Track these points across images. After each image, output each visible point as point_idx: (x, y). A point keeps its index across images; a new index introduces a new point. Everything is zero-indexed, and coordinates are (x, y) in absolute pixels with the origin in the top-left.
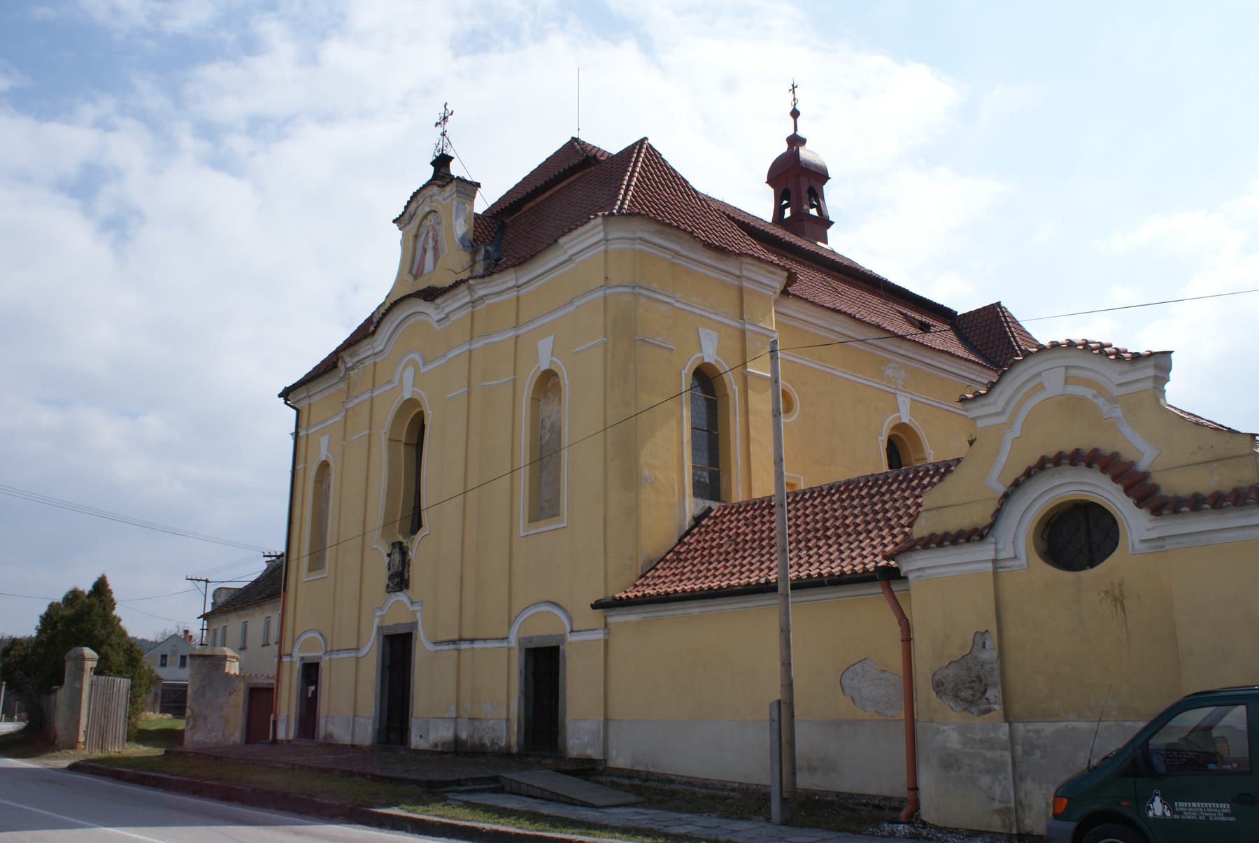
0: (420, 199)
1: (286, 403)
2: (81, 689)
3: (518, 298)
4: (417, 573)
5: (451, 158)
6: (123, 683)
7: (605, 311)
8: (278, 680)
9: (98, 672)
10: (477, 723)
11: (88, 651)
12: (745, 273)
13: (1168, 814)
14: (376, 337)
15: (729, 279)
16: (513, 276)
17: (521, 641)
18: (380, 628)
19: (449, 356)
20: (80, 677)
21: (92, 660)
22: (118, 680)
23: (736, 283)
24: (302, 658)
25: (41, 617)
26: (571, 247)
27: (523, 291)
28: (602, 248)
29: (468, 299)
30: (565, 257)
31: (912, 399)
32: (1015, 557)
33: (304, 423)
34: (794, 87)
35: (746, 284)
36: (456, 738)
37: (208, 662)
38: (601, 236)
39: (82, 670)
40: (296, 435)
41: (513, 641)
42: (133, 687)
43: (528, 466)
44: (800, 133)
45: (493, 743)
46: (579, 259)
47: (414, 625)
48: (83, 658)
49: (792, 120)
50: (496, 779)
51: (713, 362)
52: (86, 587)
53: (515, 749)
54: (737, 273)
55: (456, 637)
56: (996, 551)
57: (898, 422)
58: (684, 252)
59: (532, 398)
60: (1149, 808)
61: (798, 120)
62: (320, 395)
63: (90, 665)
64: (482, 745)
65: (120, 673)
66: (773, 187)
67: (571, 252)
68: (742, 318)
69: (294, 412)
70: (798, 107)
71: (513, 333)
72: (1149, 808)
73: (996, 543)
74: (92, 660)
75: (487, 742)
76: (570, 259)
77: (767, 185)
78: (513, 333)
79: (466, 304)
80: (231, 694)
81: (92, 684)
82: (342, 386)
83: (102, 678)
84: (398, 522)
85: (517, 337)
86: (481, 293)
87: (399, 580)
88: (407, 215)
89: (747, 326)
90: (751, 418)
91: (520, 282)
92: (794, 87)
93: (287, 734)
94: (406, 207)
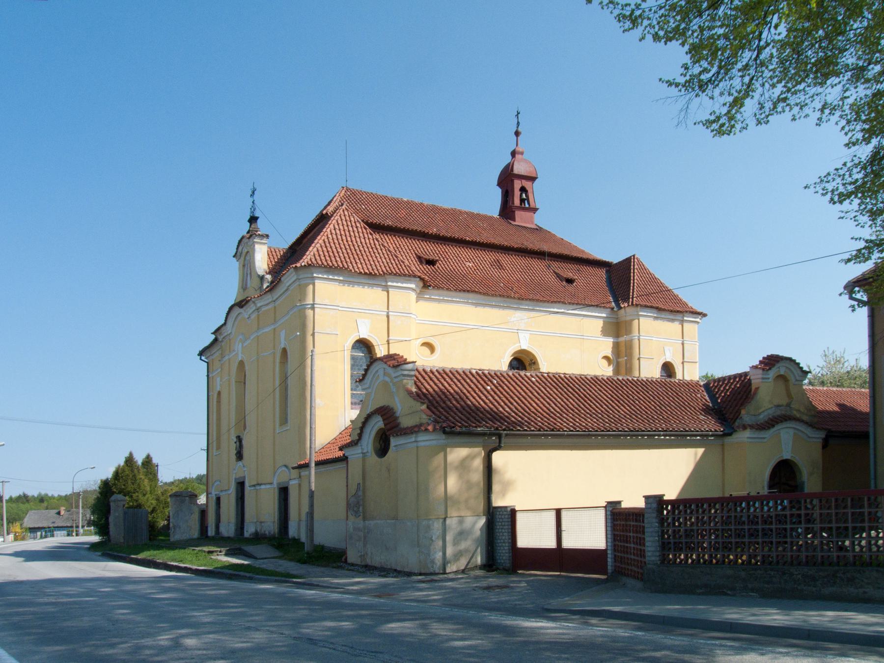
0: (242, 243)
1: (201, 359)
3: (275, 307)
4: (246, 452)
8: (207, 506)
10: (263, 524)
12: (389, 284)
14: (227, 324)
16: (270, 296)
17: (279, 484)
18: (235, 479)
19: (252, 338)
24: (216, 495)
25: (101, 481)
26: (288, 281)
27: (278, 303)
28: (298, 283)
29: (254, 308)
30: (284, 289)
31: (530, 334)
32: (368, 452)
33: (211, 370)
34: (518, 113)
36: (256, 531)
37: (179, 498)
40: (208, 376)
41: (275, 485)
44: (520, 149)
45: (269, 533)
46: (291, 288)
47: (244, 477)
49: (516, 138)
50: (240, 549)
52: (122, 462)
53: (277, 536)
55: (255, 483)
56: (362, 449)
57: (520, 349)
59: (280, 362)
61: (519, 138)
62: (216, 353)
64: (265, 534)
66: (501, 188)
67: (288, 284)
69: (206, 364)
70: (520, 129)
71: (273, 327)
73: (361, 446)
75: (267, 532)
76: (287, 290)
77: (498, 187)
78: (273, 327)
79: (254, 311)
80: (192, 514)
82: (220, 352)
84: (233, 429)
85: (274, 329)
86: (259, 305)
87: (240, 456)
88: (238, 253)
91: (274, 299)
92: (518, 113)
93: (211, 533)
94: (237, 249)
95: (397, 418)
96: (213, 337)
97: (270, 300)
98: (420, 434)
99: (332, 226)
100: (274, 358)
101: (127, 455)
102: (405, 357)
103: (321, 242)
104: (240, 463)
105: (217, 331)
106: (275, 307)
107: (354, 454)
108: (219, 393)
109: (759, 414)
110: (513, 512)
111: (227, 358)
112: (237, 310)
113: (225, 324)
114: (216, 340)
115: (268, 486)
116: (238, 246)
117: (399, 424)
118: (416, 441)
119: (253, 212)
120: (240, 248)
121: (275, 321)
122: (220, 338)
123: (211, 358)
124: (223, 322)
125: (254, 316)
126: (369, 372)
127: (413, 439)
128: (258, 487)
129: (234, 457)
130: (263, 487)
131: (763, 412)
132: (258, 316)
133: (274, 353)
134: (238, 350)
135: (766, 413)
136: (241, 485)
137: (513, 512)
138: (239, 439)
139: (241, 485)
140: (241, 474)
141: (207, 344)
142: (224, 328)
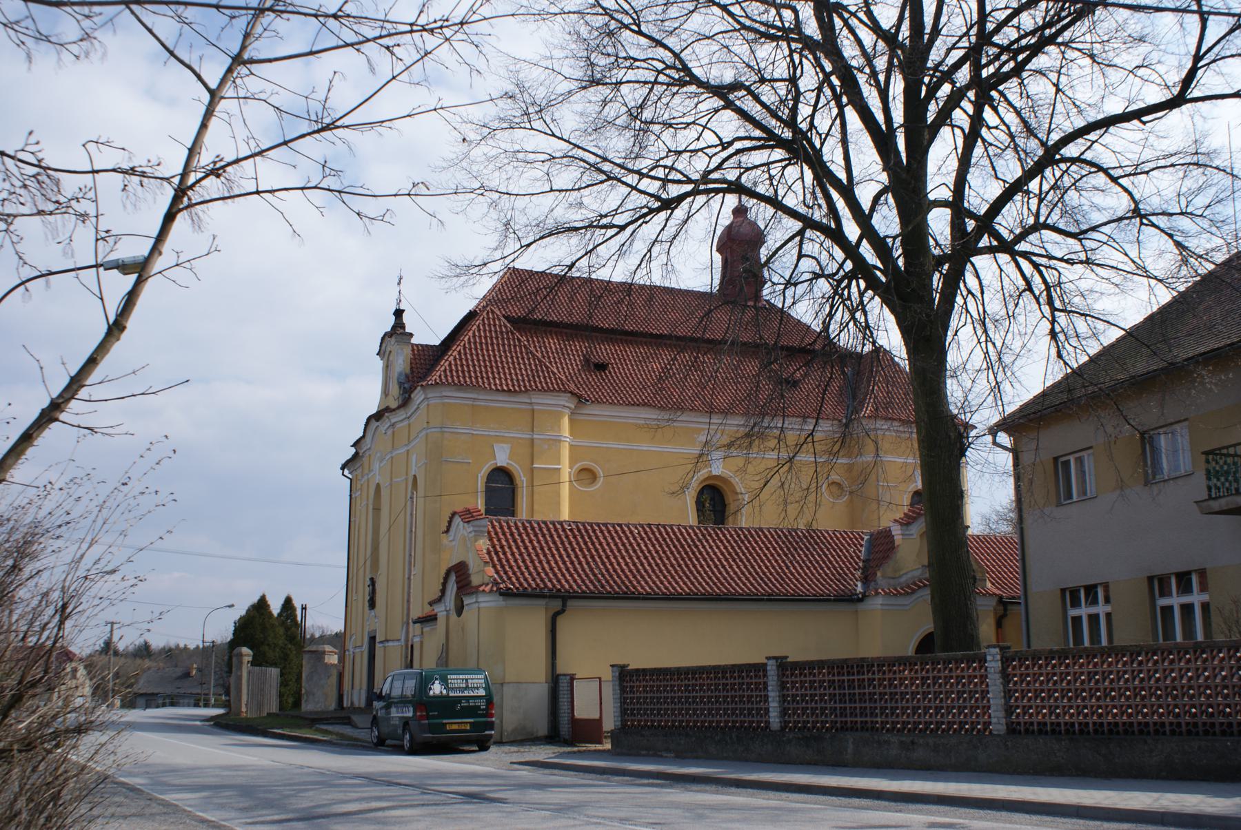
2: (241, 676)
3: (409, 425)
5: (403, 311)
6: (274, 672)
7: (427, 444)
9: (255, 663)
11: (245, 650)
12: (533, 401)
13: (444, 692)
15: (523, 406)
20: (240, 668)
21: (248, 655)
22: (269, 669)
23: (529, 407)
27: (412, 420)
35: (535, 407)
38: (423, 397)
39: (241, 663)
42: (282, 675)
43: (1124, 333)
48: (241, 655)
51: (505, 465)
54: (528, 401)
58: (481, 397)
60: (430, 689)
63: (247, 659)
65: (274, 665)
68: (533, 431)
71: (406, 448)
72: (430, 689)
74: (248, 655)
76: (418, 408)
78: (406, 448)
81: (249, 673)
83: (257, 668)
86: (393, 421)
89: (535, 436)
90: (536, 497)
94: (381, 346)
95: (469, 576)
96: (353, 450)
97: (404, 416)
98: (480, 595)
99: (471, 334)
100: (407, 484)
101: (255, 599)
102: (182, 645)
103: (455, 353)
104: (373, 613)
105: (356, 444)
106: (409, 425)
107: (440, 609)
108: (415, 476)
109: (900, 577)
110: (572, 678)
111: (366, 478)
112: (374, 424)
113: (364, 436)
114: (356, 456)
115: (396, 643)
116: (381, 343)
117: (470, 582)
118: (477, 602)
119: (398, 304)
120: (384, 345)
121: (409, 442)
122: (361, 452)
123: (355, 473)
124: (361, 434)
125: (390, 432)
126: (453, 524)
127: (474, 600)
128: (387, 644)
129: (367, 604)
130: (390, 644)
131: (906, 573)
132: (393, 432)
133: (406, 479)
134: (377, 472)
135: (909, 575)
136: (372, 639)
137: (572, 678)
138: (373, 581)
139: (372, 639)
140: (372, 628)
141: (349, 456)
142: (363, 441)
